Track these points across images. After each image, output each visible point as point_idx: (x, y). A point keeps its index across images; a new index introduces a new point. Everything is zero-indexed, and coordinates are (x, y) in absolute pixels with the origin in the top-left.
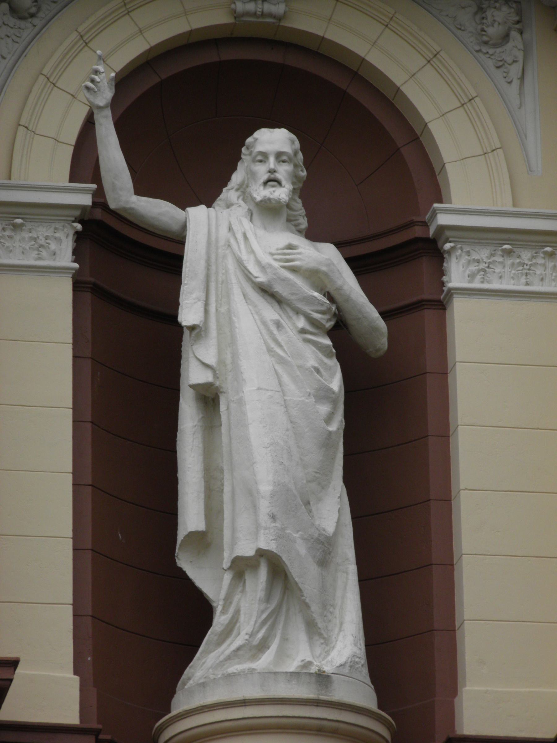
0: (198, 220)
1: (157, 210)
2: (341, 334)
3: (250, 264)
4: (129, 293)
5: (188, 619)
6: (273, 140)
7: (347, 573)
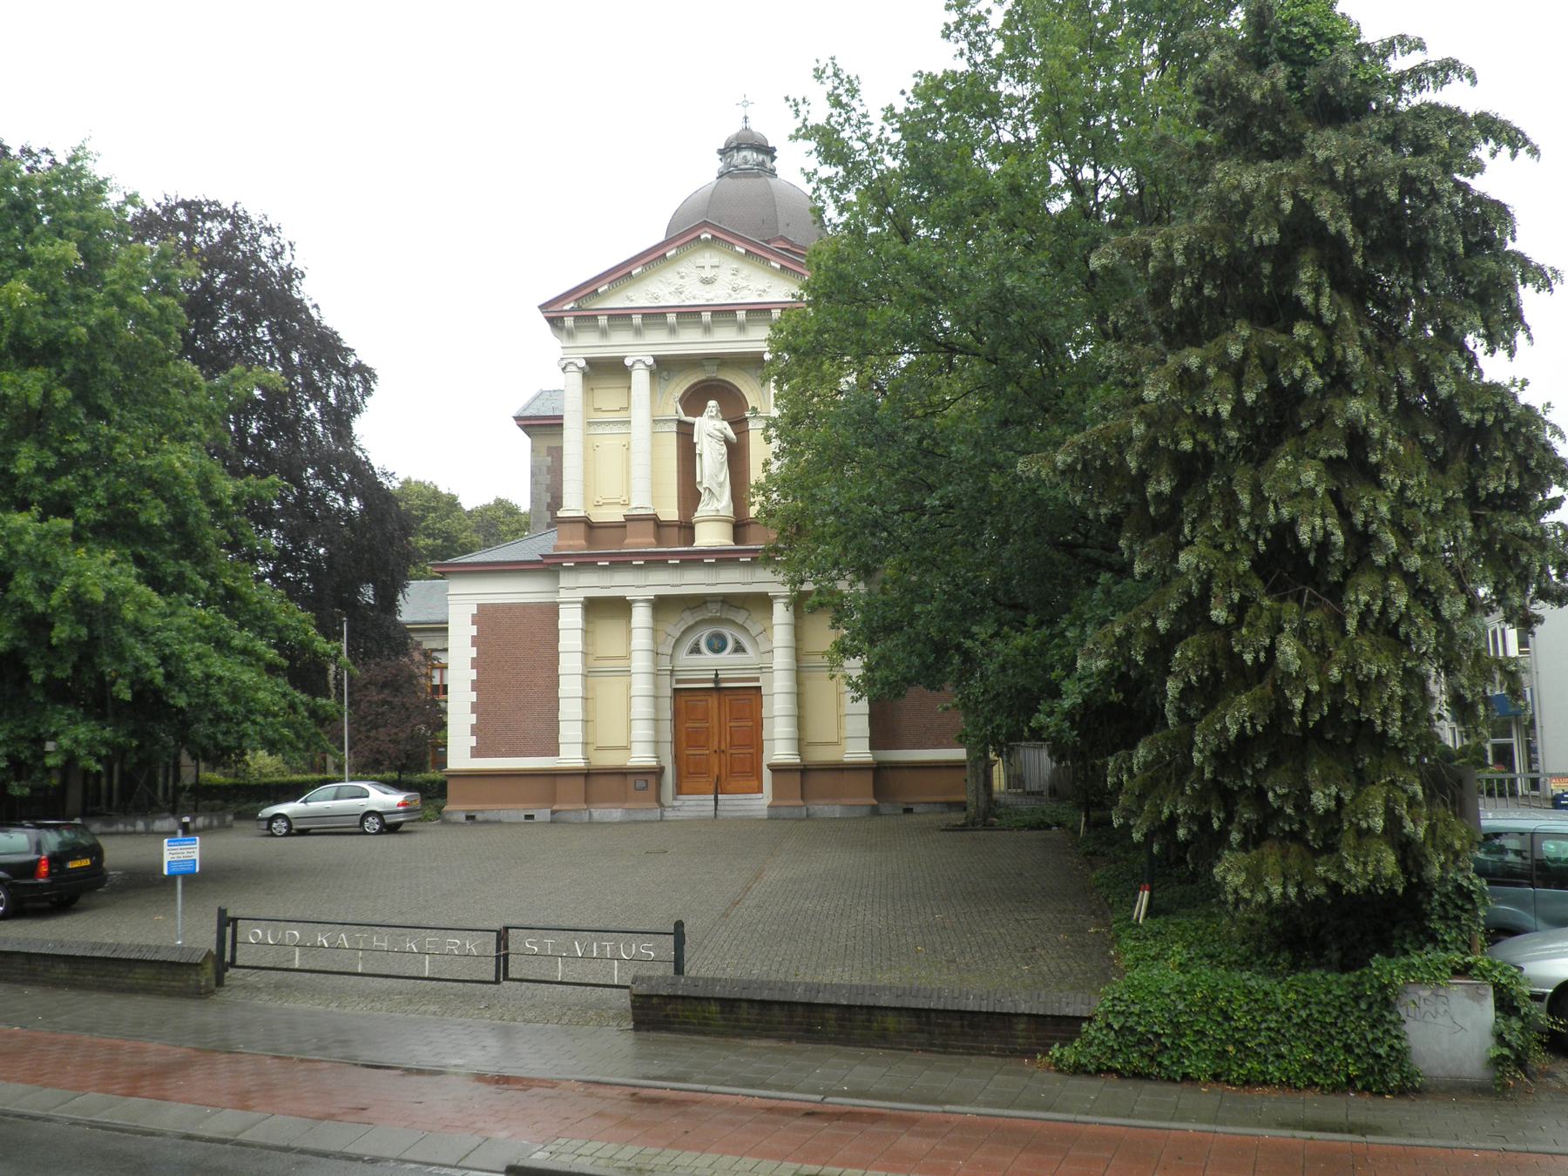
0: (697, 421)
1: (690, 419)
2: (727, 441)
3: (710, 427)
4: (685, 433)
5: (697, 496)
6: (712, 403)
7: (628, 672)
